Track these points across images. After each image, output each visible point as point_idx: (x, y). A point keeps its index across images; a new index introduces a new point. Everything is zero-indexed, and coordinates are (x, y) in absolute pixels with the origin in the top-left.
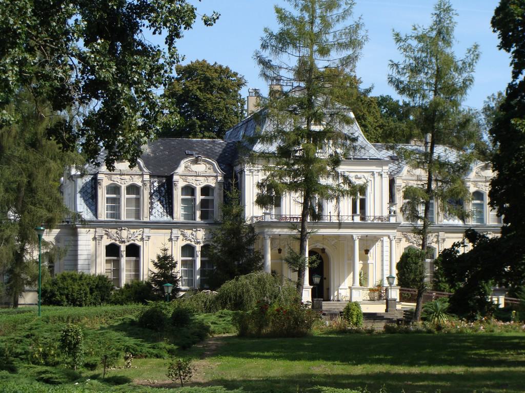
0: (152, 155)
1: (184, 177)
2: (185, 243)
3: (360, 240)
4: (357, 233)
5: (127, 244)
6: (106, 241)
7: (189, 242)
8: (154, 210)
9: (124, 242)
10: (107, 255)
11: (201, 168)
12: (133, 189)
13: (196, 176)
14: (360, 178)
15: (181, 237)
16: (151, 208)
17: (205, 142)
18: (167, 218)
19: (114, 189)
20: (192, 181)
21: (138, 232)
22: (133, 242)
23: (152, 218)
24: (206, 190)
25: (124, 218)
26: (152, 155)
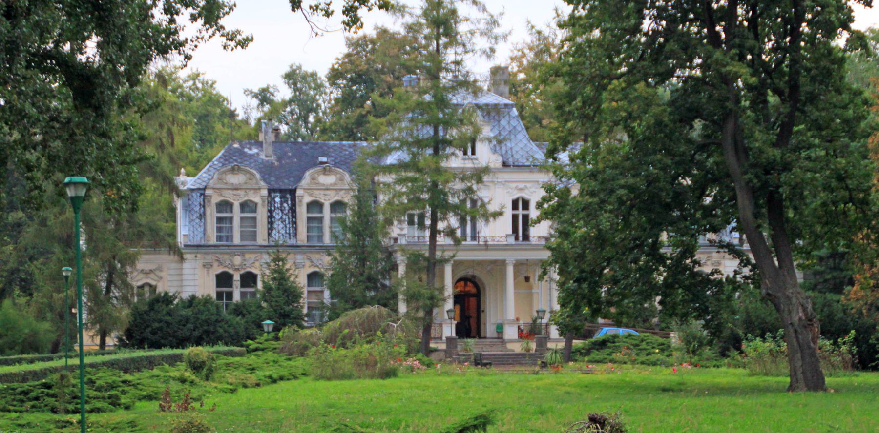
0: (276, 163)
1: (310, 191)
3: (515, 266)
5: (242, 272)
7: (317, 269)
8: (274, 231)
11: (328, 180)
15: (308, 263)
16: (271, 229)
17: (344, 145)
19: (316, 205)
20: (229, 196)
24: (337, 206)
26: (276, 163)
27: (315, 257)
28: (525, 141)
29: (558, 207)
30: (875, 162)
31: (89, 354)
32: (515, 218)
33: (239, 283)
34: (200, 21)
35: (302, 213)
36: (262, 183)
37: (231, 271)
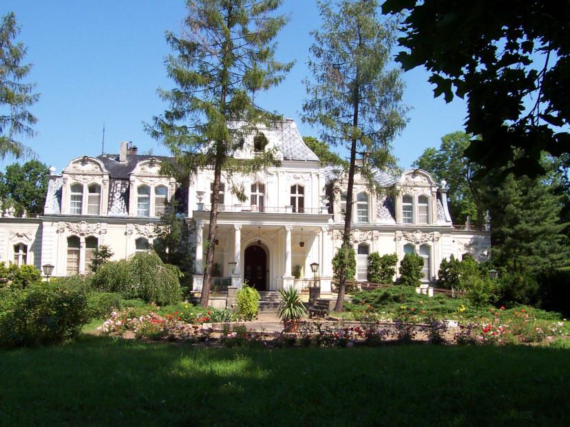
2: (138, 236)
3: (242, 231)
4: (289, 225)
5: (86, 236)
6: (68, 234)
9: (418, 243)
10: (69, 246)
12: (423, 199)
13: (150, 177)
14: (299, 178)
15: (135, 232)
18: (125, 214)
20: (80, 179)
21: (94, 226)
22: (91, 234)
23: (110, 214)
25: (85, 212)
27: (141, 228)
28: (301, 144)
29: (492, 341)
30: (166, 149)
31: (147, 213)
32: (293, 199)
33: (85, 244)
34: (515, 273)
35: (134, 195)
36: (105, 171)
37: (78, 235)
